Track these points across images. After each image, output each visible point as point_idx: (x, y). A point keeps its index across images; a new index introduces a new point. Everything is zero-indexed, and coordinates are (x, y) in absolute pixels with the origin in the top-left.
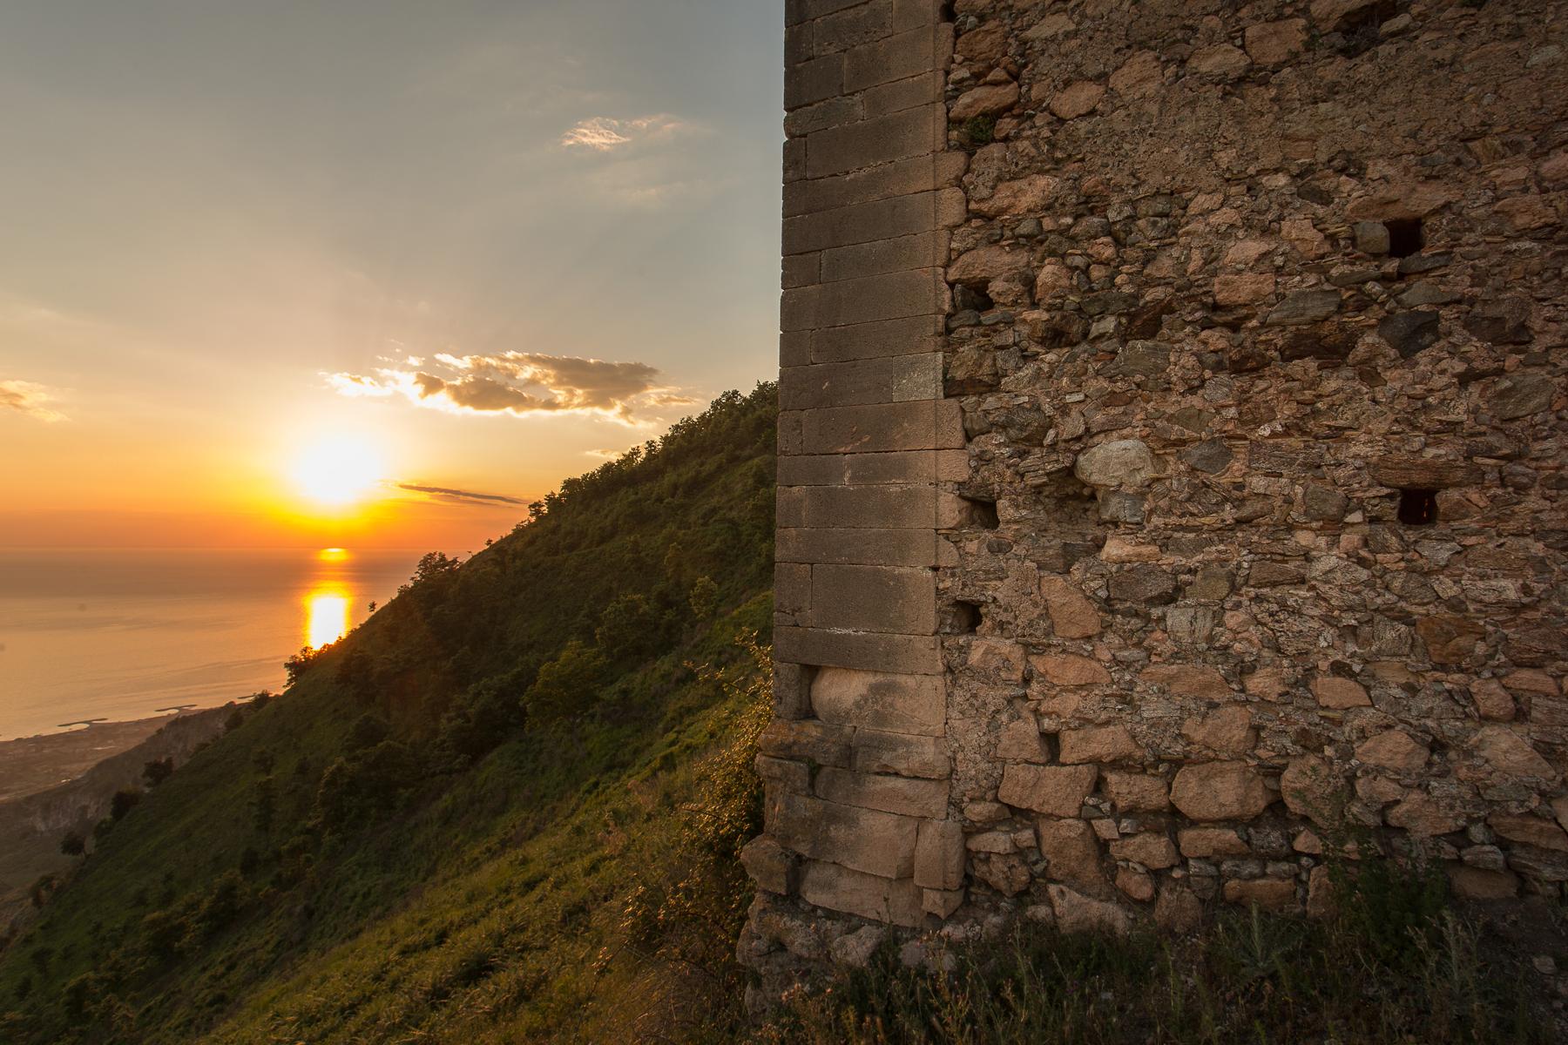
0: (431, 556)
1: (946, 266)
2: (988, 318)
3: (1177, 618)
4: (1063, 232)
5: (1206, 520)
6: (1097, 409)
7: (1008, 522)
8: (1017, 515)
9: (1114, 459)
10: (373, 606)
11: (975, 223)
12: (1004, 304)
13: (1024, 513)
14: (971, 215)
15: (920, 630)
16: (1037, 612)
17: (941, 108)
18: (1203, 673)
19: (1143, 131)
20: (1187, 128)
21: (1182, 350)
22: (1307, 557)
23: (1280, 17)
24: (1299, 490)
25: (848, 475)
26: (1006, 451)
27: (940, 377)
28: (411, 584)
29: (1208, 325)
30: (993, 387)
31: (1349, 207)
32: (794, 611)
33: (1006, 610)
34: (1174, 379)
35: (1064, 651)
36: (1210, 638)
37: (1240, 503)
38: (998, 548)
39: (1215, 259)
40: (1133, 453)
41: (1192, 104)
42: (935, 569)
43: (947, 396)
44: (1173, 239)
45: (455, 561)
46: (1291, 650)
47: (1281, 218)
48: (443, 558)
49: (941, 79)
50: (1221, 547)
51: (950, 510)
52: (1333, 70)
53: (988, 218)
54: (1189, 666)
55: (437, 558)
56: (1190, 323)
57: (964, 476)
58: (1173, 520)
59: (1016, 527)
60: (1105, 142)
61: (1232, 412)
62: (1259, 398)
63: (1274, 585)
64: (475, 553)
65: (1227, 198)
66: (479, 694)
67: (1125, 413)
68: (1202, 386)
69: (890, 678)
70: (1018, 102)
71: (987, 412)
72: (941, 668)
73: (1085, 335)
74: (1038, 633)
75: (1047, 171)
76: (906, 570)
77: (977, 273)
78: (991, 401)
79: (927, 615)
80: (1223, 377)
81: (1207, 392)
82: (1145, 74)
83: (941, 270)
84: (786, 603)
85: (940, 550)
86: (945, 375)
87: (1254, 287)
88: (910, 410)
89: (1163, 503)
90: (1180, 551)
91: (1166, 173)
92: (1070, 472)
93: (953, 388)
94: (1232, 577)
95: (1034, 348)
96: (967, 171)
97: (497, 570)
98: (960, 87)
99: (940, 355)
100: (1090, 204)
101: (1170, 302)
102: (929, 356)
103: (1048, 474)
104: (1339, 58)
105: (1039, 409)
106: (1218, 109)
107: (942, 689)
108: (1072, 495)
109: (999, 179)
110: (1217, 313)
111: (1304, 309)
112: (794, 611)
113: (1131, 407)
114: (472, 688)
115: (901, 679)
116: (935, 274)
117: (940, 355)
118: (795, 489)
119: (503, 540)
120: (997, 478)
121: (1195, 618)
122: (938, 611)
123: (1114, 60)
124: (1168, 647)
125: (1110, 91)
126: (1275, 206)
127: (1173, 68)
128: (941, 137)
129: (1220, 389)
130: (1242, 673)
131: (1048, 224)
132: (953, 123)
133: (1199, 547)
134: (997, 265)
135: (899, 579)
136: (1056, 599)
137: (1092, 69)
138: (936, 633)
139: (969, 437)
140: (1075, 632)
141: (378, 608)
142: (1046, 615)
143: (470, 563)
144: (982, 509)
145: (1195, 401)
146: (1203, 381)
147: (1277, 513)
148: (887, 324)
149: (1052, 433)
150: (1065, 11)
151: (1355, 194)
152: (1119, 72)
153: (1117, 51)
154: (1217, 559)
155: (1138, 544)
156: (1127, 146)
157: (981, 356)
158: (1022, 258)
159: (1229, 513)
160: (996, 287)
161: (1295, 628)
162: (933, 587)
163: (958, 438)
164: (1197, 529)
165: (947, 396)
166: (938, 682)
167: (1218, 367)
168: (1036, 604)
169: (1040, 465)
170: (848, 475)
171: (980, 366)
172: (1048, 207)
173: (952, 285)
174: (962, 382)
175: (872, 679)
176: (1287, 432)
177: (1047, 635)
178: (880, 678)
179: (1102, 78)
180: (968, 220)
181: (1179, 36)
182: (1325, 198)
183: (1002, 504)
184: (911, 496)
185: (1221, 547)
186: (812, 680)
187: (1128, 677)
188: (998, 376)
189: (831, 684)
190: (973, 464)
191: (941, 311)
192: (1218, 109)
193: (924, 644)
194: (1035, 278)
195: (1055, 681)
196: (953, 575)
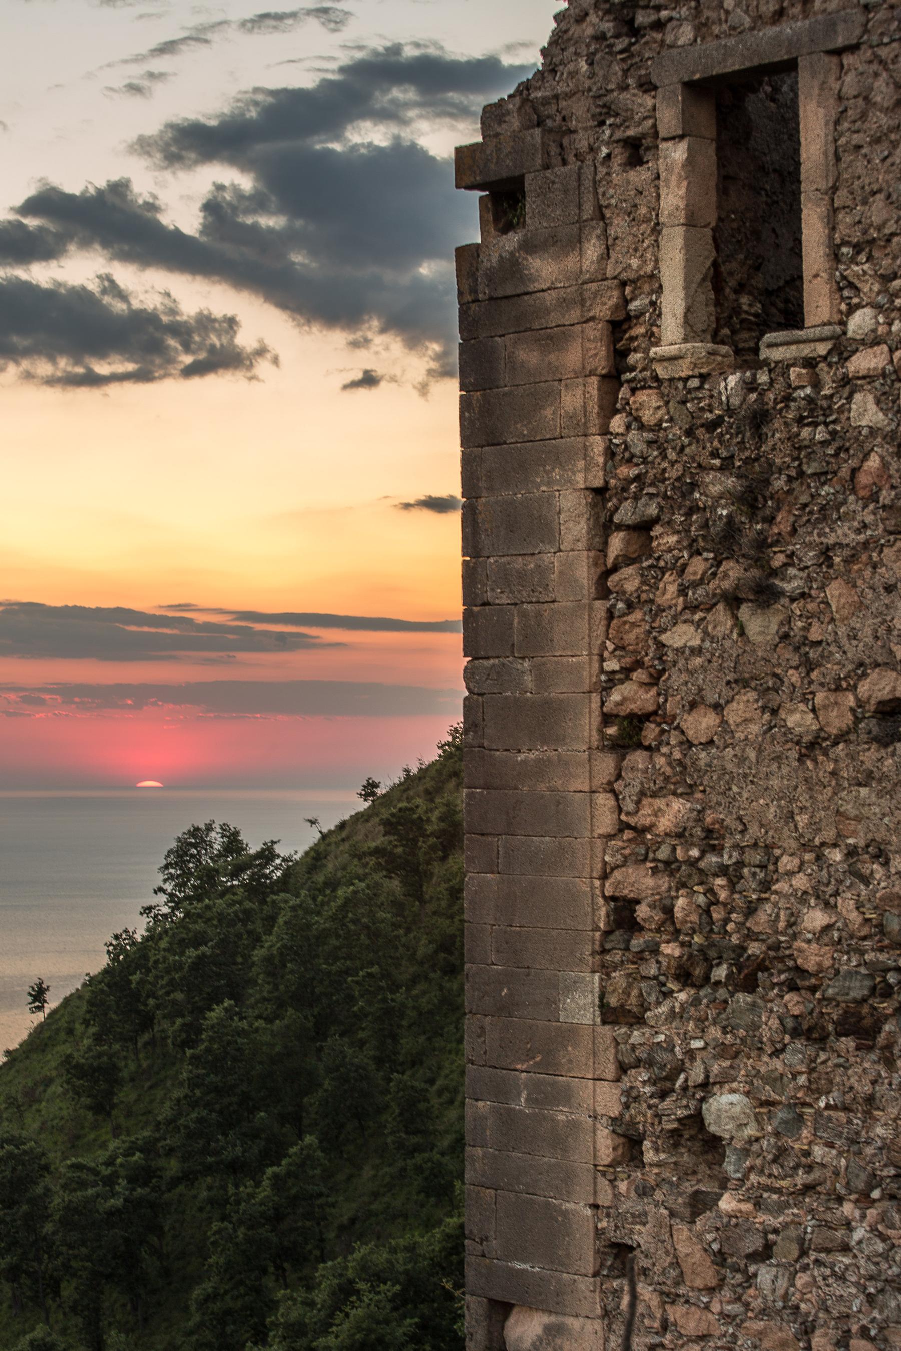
0: (197, 837)
1: (604, 877)
2: (637, 943)
3: (765, 1275)
4: (693, 863)
5: (783, 1183)
6: (715, 1057)
7: (651, 1165)
8: (655, 1159)
9: (727, 1108)
10: (38, 995)
11: (628, 834)
12: (650, 930)
13: (663, 1156)
14: (624, 826)
15: (582, 1271)
16: (669, 1260)
17: (596, 698)
18: (781, 1330)
19: (745, 775)
20: (775, 782)
21: (772, 1011)
22: (848, 1225)
23: (838, 688)
24: (843, 1162)
25: (524, 1095)
26: (647, 1089)
27: (597, 1002)
28: (140, 928)
29: (793, 987)
30: (639, 1021)
31: (878, 895)
32: (482, 1240)
33: (646, 1256)
34: (765, 1039)
35: (687, 1302)
36: (786, 1297)
37: (809, 1168)
38: (644, 1192)
39: (794, 924)
40: (738, 1109)
41: (778, 758)
42: (595, 1207)
43: (604, 1022)
44: (767, 895)
45: (267, 854)
46: (835, 1314)
47: (837, 894)
48: (233, 843)
49: (596, 666)
50: (796, 1211)
51: (605, 1145)
52: (870, 756)
53: (640, 831)
54: (772, 1323)
55: (217, 840)
56: (777, 984)
57: (615, 1112)
58: (763, 1180)
59: (656, 1171)
60: (719, 779)
61: (802, 1080)
62: (821, 1068)
63: (828, 1251)
64: (329, 824)
65: (802, 863)
66: (346, 1293)
67: (732, 1067)
68: (783, 1050)
69: (561, 1319)
70: (655, 713)
71: (633, 1048)
72: (599, 1311)
73: (707, 978)
74: (669, 1282)
75: (681, 795)
76: (570, 1206)
77: (626, 892)
78: (636, 1036)
79: (585, 1254)
80: (798, 1044)
81: (787, 1056)
82: (748, 715)
83: (597, 883)
84: (475, 1232)
85: (599, 1188)
86: (601, 998)
87: (818, 959)
88: (571, 1033)
89: (758, 1162)
90: (769, 1211)
91: (762, 825)
92: (697, 1120)
93: (610, 1015)
94: (801, 1241)
95: (672, 985)
96: (619, 776)
97: (395, 885)
98: (612, 680)
99: (597, 977)
100: (711, 839)
101: (764, 960)
102: (587, 976)
103: (679, 1120)
104: (874, 746)
105: (672, 1051)
106: (796, 770)
107: (600, 1334)
108: (698, 1138)
109: (642, 794)
110: (798, 980)
111: (849, 988)
112: (482, 1240)
113: (737, 1061)
114: (327, 1276)
115: (570, 1321)
116: (592, 887)
117: (597, 977)
118: (480, 1104)
119: (410, 781)
120: (642, 1115)
121: (776, 1277)
122: (597, 1252)
123: (727, 692)
124: (757, 1304)
125: (724, 722)
126: (833, 881)
127: (767, 716)
128: (595, 736)
129: (797, 1055)
130: (806, 1333)
131: (680, 854)
132: (607, 719)
133: (781, 1208)
134: (641, 881)
135: (565, 1214)
136: (683, 1249)
137: (712, 697)
138: (596, 1275)
139: (623, 1069)
140: (699, 1283)
141: (52, 1003)
142: (676, 1264)
143: (316, 856)
144: (631, 1144)
145: (777, 1064)
146: (785, 1046)
147: (829, 1182)
148: (554, 933)
149: (682, 1076)
150: (692, 622)
151: (883, 884)
152: (730, 705)
153: (728, 683)
154: (793, 1222)
155: (740, 1201)
156: (735, 789)
157: (630, 985)
158: (664, 882)
159: (802, 1178)
160: (642, 911)
161: (838, 1293)
162: (591, 1226)
163: (610, 1071)
164: (779, 1191)
165: (604, 1022)
166: (598, 1325)
167: (796, 1033)
168: (667, 1253)
169: (675, 1109)
170: (524, 1095)
171: (629, 995)
172: (680, 835)
173: (607, 899)
174: (615, 1009)
175: (546, 1319)
176: (835, 1108)
177: (677, 1284)
178: (553, 1319)
179: (717, 707)
180: (621, 831)
181: (770, 684)
182: (866, 880)
183: (647, 1144)
184: (574, 1126)
185: (796, 1211)
186: (506, 1317)
187: (731, 1331)
188: (644, 1007)
189: (517, 1322)
190: (624, 1099)
191: (597, 929)
192: (796, 770)
193: (585, 1285)
194: (673, 906)
195: (683, 1332)
196: (608, 1215)
